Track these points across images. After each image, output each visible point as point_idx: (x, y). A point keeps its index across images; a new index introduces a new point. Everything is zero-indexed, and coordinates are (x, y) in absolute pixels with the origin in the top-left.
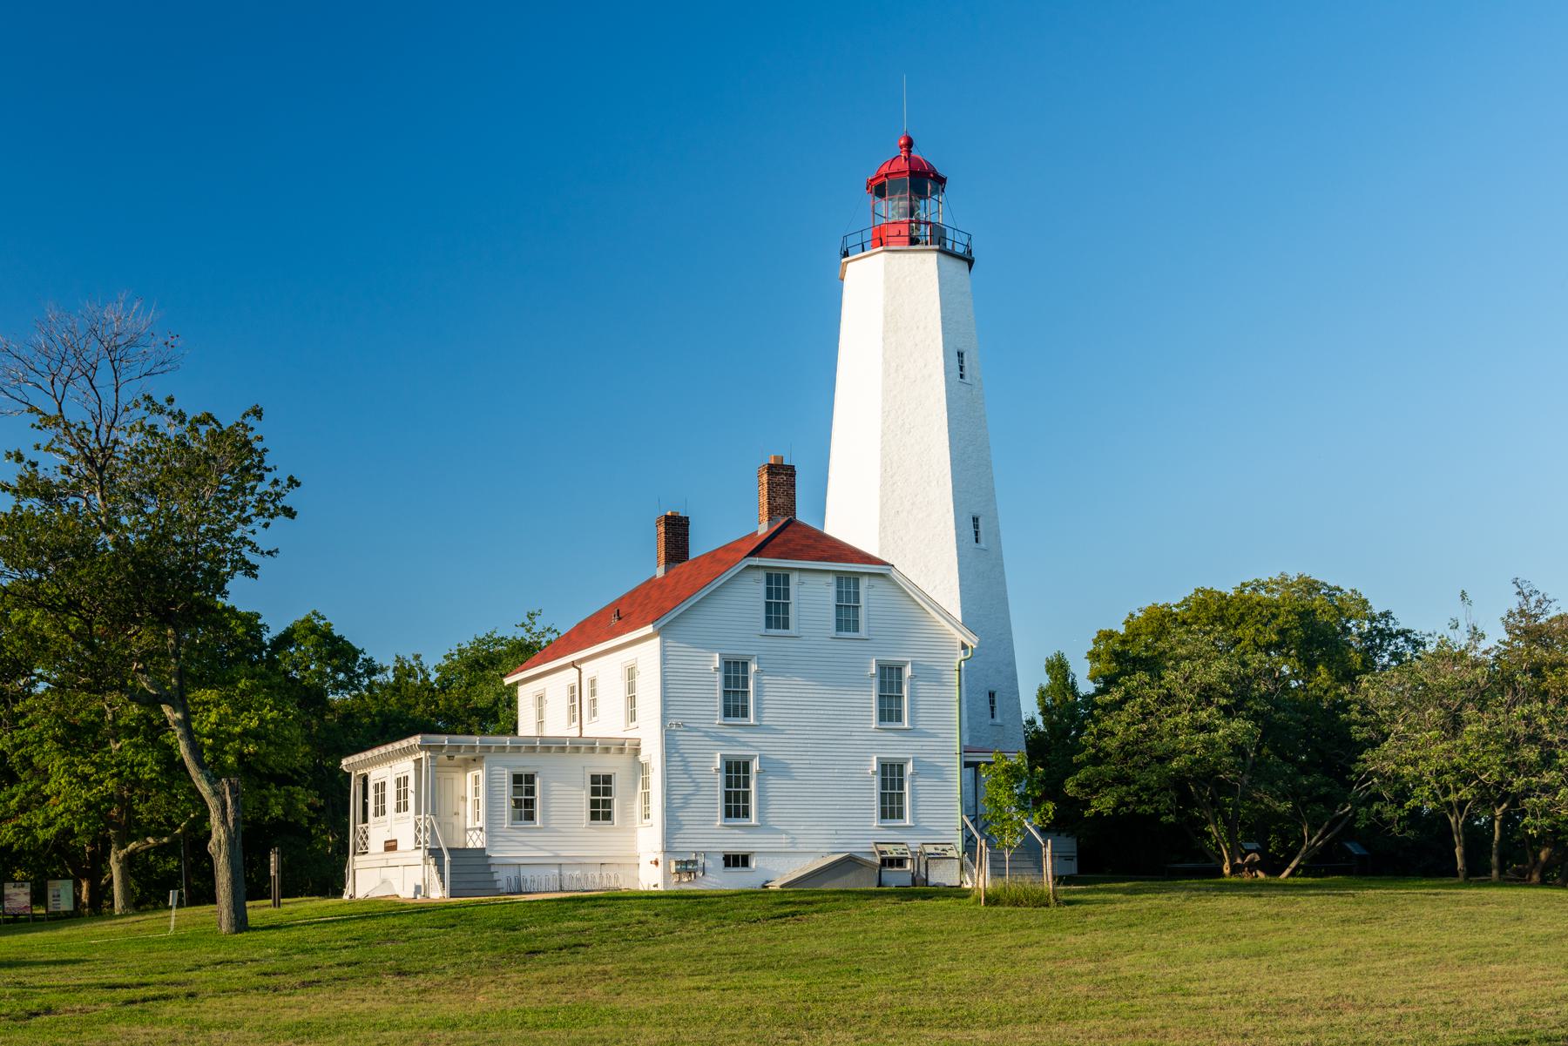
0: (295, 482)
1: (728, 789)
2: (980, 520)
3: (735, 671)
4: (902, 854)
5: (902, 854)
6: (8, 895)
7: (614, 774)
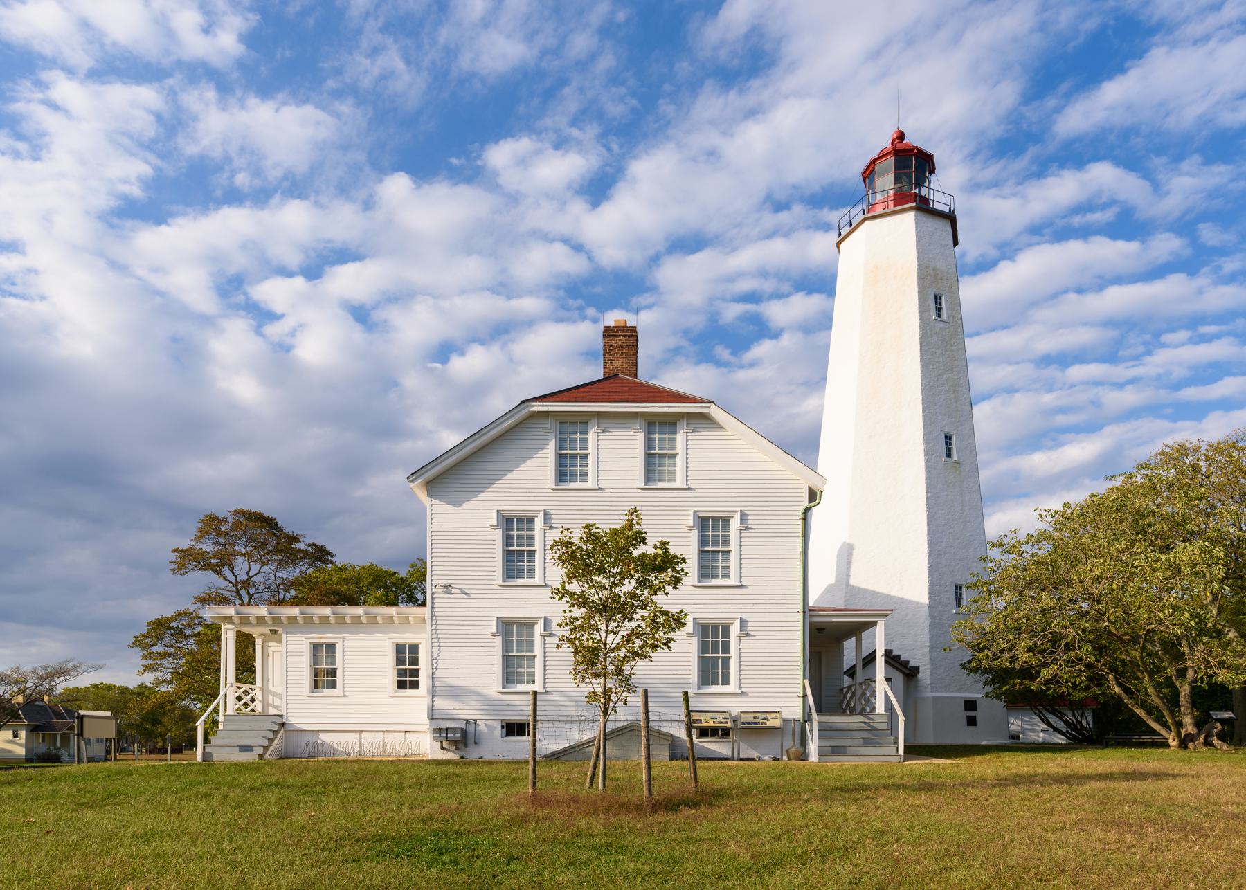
0: (821, 629)
2: (954, 439)
4: (721, 722)
5: (721, 722)
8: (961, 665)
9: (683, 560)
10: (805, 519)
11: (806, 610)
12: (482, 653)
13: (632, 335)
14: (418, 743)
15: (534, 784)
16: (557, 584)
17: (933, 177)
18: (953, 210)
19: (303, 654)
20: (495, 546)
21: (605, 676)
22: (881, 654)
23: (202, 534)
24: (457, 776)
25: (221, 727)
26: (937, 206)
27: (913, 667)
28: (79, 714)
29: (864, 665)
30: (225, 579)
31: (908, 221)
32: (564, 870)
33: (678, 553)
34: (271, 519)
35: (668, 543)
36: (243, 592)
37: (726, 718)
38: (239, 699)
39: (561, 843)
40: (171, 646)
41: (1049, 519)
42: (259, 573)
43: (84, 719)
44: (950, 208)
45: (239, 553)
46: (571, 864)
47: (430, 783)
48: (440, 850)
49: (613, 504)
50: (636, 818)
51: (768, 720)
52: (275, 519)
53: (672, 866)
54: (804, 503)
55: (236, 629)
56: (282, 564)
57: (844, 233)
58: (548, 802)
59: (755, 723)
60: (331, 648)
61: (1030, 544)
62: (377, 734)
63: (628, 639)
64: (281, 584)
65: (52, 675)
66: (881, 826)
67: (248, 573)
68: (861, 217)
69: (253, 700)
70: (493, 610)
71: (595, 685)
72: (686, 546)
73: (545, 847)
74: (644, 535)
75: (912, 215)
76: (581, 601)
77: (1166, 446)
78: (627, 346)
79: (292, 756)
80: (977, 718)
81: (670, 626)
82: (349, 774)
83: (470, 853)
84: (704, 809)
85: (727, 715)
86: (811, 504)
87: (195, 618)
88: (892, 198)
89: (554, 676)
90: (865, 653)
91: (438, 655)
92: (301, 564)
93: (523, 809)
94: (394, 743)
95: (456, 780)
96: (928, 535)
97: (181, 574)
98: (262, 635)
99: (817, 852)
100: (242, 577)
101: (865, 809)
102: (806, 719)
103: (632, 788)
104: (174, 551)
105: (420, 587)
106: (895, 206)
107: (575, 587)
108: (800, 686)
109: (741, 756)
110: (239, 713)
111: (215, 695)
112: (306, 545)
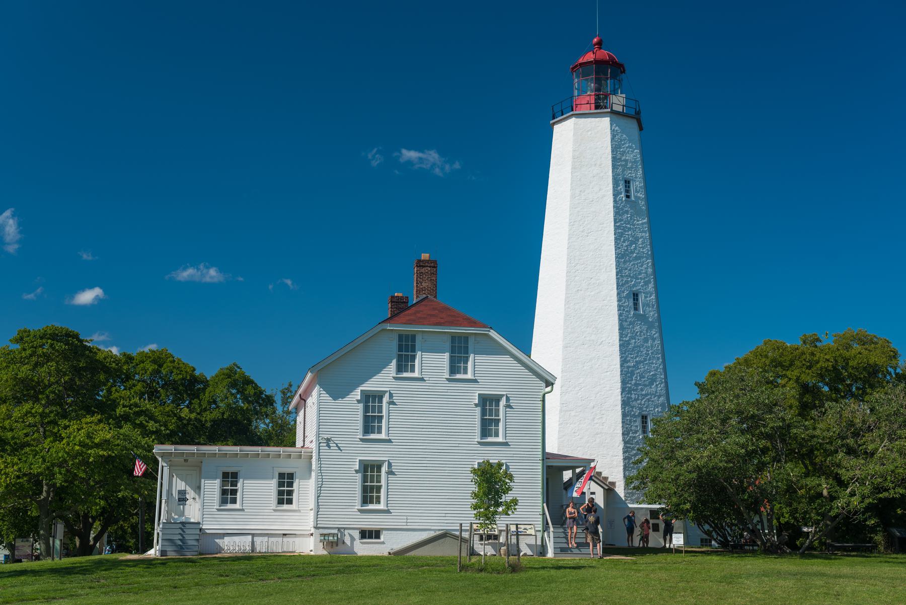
1: (364, 484)
3: (371, 400)
6: (18, 547)
7: (295, 472)
20: (359, 413)
78: (431, 274)
79: (204, 553)
80: (660, 525)
96: (621, 374)
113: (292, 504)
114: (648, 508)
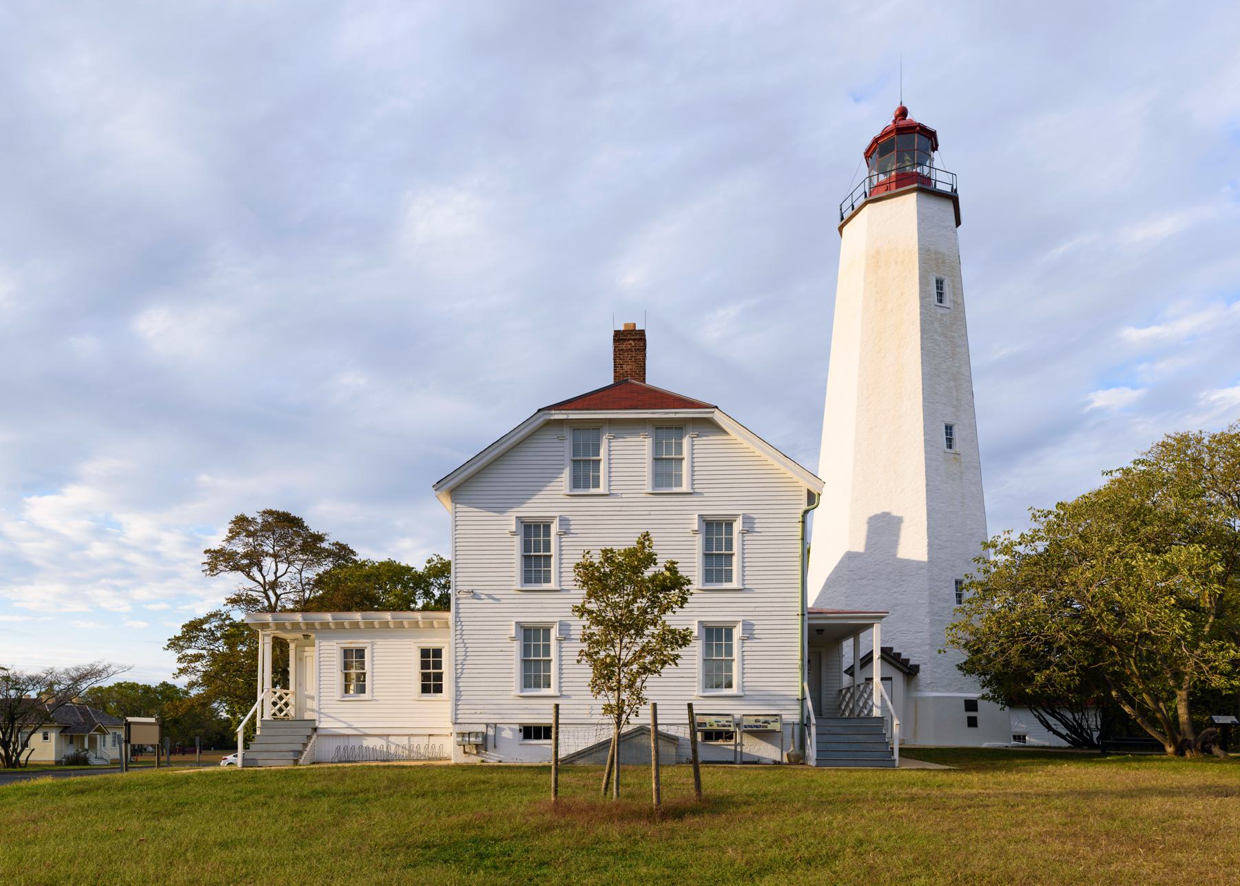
8: (958, 665)
9: (689, 581)
10: (803, 522)
11: (805, 613)
12: (502, 657)
13: (641, 339)
14: (441, 746)
15: (556, 792)
16: (579, 603)
17: (935, 155)
18: (956, 190)
19: (335, 659)
21: (618, 689)
22: (877, 657)
23: (234, 535)
24: (484, 782)
25: (258, 733)
26: (940, 186)
27: (913, 665)
28: (127, 720)
29: (862, 666)
30: (254, 580)
31: (908, 205)
32: (588, 873)
33: (684, 574)
34: (298, 519)
35: (677, 563)
36: (270, 593)
37: (730, 722)
38: (275, 704)
39: (583, 849)
40: (204, 649)
41: (1043, 519)
42: (285, 573)
43: (132, 726)
44: (952, 187)
45: (267, 554)
46: (594, 869)
47: (458, 790)
48: (481, 856)
49: (623, 509)
50: (646, 825)
51: (769, 723)
52: (301, 519)
53: (678, 870)
54: (803, 506)
55: (272, 635)
56: (307, 564)
57: (846, 216)
58: (569, 809)
59: (757, 727)
60: (360, 653)
61: (1023, 545)
62: (403, 737)
63: (638, 656)
64: (307, 584)
65: (84, 677)
66: (861, 835)
67: (275, 573)
68: (862, 200)
69: (286, 705)
70: (512, 614)
71: (610, 697)
72: (692, 567)
73: (569, 853)
74: (654, 557)
75: (914, 196)
76: (598, 620)
77: (1168, 436)
78: (636, 350)
81: (677, 643)
82: (386, 781)
83: (507, 858)
84: (707, 817)
85: (730, 719)
86: (809, 507)
87: (225, 619)
88: (894, 179)
89: (570, 680)
90: (862, 654)
91: (465, 660)
92: (325, 563)
93: (548, 817)
94: (418, 746)
95: (482, 786)
97: (212, 575)
98: (295, 639)
99: (803, 859)
100: (271, 578)
101: (851, 818)
102: (805, 722)
103: (643, 796)
104: (206, 552)
105: (436, 582)
106: (897, 188)
107: (593, 606)
108: (800, 689)
109: (744, 760)
110: (274, 719)
111: (254, 698)
112: (330, 544)
113: (442, 692)
114: (962, 697)
